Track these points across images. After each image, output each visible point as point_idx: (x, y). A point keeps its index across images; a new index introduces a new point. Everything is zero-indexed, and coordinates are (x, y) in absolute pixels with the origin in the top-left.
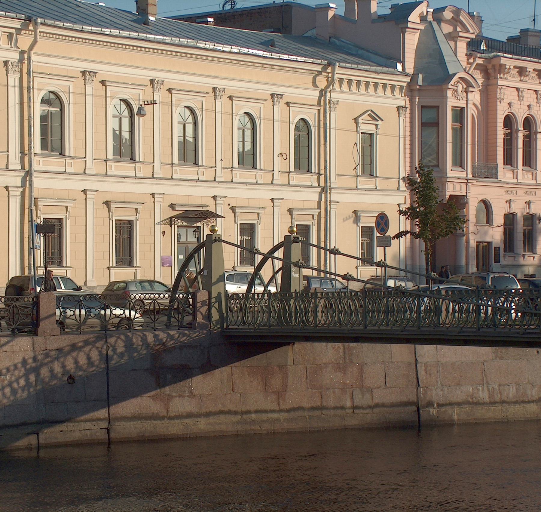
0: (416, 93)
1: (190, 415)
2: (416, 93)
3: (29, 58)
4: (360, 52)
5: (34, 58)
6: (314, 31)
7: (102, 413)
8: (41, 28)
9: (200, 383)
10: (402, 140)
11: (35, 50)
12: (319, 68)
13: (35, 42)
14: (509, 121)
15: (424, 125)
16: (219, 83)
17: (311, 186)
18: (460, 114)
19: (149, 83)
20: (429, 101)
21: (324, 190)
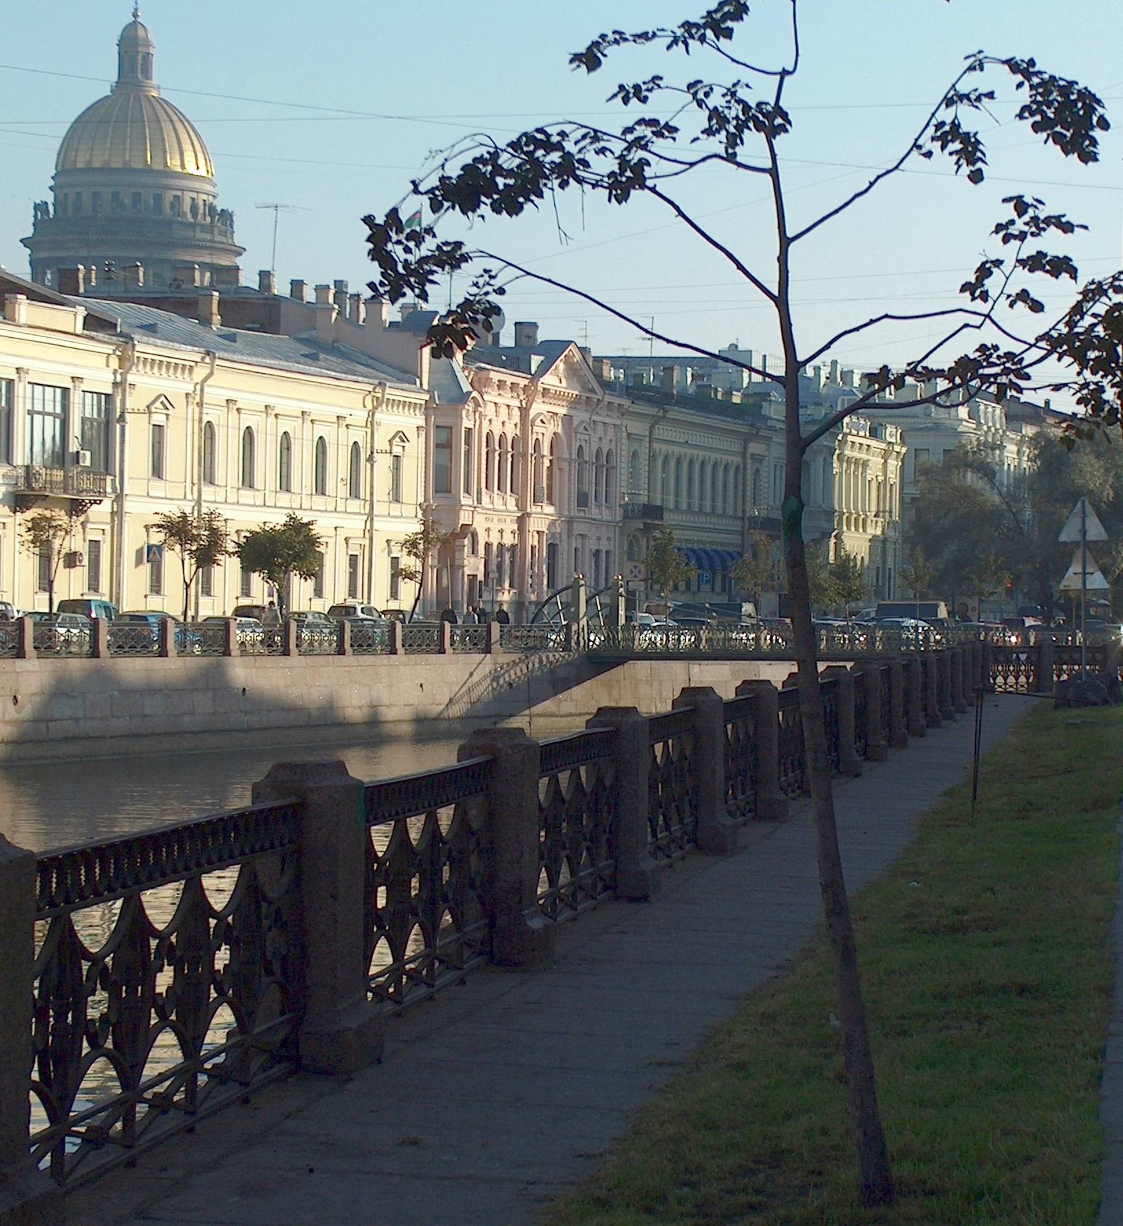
0: (431, 411)
1: (571, 715)
2: (431, 411)
3: (202, 390)
4: (371, 362)
5: (206, 389)
6: (314, 333)
7: (527, 712)
8: (218, 362)
9: (577, 692)
10: (190, 423)
11: (209, 382)
12: (370, 388)
13: (211, 374)
14: (489, 436)
15: (437, 446)
16: (306, 407)
17: (360, 514)
18: (469, 431)
19: (224, 403)
20: (443, 421)
21: (371, 516)
